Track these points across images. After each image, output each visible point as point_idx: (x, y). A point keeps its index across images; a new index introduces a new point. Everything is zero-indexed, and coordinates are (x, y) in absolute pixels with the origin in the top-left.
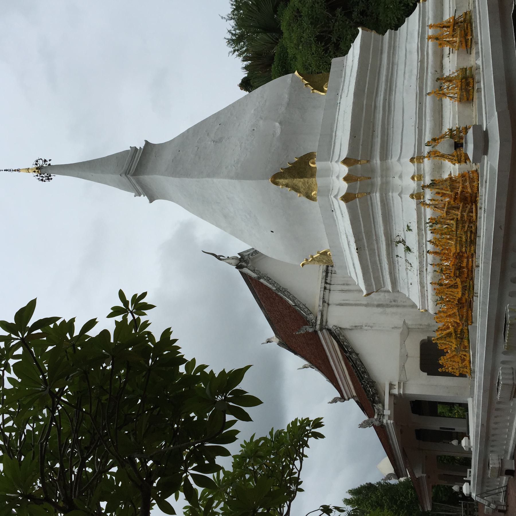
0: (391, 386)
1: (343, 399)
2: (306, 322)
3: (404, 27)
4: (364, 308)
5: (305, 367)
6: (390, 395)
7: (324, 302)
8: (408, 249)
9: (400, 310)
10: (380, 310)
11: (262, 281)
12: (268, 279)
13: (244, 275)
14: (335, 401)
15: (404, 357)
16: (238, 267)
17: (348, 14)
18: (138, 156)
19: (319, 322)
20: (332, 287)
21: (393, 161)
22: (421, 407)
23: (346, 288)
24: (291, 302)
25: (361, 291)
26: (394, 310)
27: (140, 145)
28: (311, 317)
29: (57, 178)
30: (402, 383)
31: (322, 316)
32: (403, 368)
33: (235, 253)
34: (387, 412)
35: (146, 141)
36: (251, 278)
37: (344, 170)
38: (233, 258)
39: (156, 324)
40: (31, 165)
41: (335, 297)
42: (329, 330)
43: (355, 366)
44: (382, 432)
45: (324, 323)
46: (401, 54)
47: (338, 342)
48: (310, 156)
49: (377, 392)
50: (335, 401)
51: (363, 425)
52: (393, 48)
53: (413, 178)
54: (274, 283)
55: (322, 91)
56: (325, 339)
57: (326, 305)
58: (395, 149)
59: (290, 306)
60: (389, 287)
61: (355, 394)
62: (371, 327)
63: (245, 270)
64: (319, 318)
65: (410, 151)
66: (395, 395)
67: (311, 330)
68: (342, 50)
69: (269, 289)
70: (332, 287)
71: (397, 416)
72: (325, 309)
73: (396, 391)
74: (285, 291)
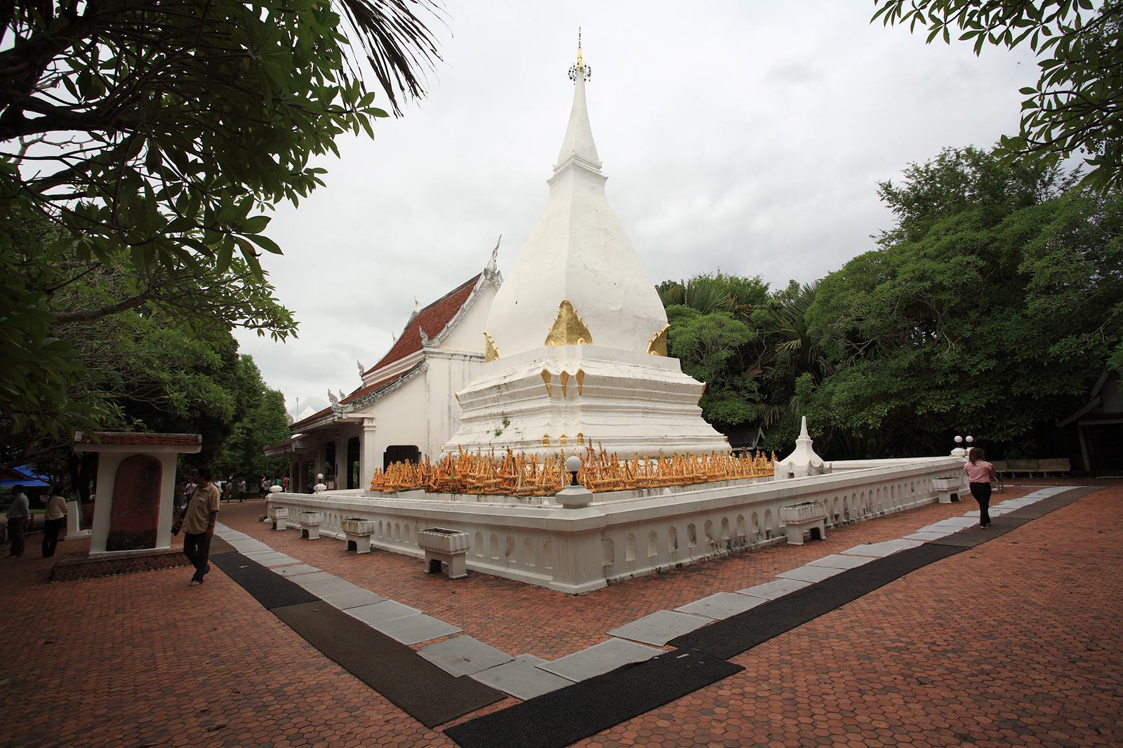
0: (372, 419)
6: (363, 419)
7: (452, 355)
10: (446, 408)
14: (360, 367)
18: (594, 170)
19: (432, 350)
26: (446, 421)
31: (438, 353)
35: (607, 178)
41: (457, 365)
42: (424, 360)
45: (431, 355)
50: (360, 367)
57: (449, 357)
61: (367, 386)
62: (429, 400)
63: (483, 278)
64: (436, 350)
66: (363, 423)
72: (445, 356)
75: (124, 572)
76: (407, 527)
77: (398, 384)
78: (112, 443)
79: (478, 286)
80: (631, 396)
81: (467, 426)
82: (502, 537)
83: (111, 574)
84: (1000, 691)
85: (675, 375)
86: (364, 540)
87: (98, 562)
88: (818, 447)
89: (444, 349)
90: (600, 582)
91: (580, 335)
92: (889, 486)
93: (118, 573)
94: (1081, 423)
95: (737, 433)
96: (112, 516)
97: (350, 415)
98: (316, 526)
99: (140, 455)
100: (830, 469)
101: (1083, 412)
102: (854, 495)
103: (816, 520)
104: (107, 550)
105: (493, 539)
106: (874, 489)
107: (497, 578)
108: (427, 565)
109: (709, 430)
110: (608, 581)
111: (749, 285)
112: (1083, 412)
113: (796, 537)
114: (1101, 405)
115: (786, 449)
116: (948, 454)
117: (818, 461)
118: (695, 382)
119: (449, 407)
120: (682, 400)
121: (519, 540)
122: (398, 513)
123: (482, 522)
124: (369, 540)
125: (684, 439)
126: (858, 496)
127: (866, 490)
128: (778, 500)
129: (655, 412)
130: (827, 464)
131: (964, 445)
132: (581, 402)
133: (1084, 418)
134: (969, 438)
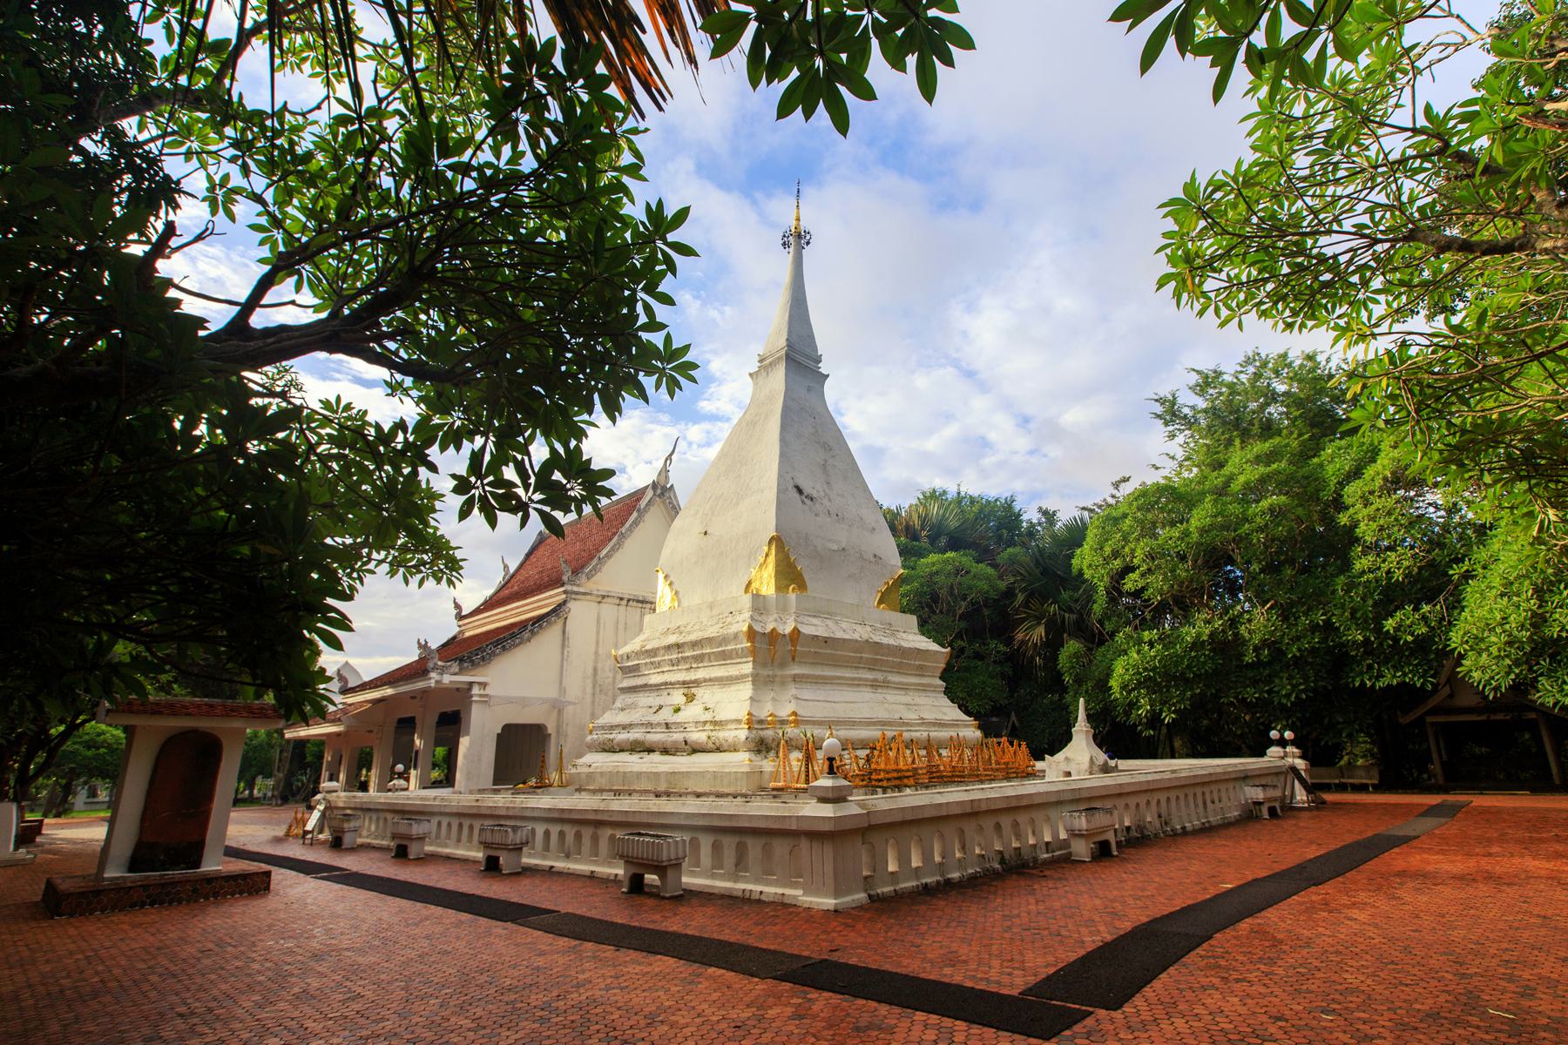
0: (484, 685)
1: (460, 617)
2: (576, 572)
3: (946, 701)
4: (593, 650)
5: (506, 567)
6: (471, 684)
8: (677, 710)
9: (588, 698)
10: (590, 671)
11: (635, 514)
12: (636, 523)
13: (642, 491)
14: (457, 606)
15: (524, 702)
16: (654, 485)
17: (959, 636)
18: (811, 364)
20: (622, 608)
21: (792, 690)
22: (451, 723)
23: (621, 627)
24: (604, 552)
25: (616, 647)
26: (589, 690)
27: (824, 368)
28: (583, 578)
29: (788, 258)
30: (486, 700)
32: (510, 701)
33: (673, 479)
34: (447, 679)
36: (638, 500)
37: (788, 629)
38: (667, 477)
39: (1017, 506)
40: (804, 225)
41: (609, 610)
42: (565, 602)
43: (513, 636)
44: (417, 670)
46: (848, 694)
47: (547, 614)
48: (802, 586)
49: (474, 665)
50: (457, 606)
51: (423, 646)
52: (923, 689)
53: (794, 713)
54: (630, 529)
55: (880, 602)
56: (552, 597)
58: (807, 693)
59: (598, 551)
60: (625, 684)
61: (467, 634)
63: (650, 493)
65: (806, 711)
66: (470, 689)
67: (565, 578)
68: (924, 627)
69: (623, 524)
70: (622, 608)
71: (441, 691)
73: (476, 690)
74: (619, 545)
75: (161, 904)
76: (578, 836)
77: (526, 635)
78: (161, 713)
79: (643, 503)
80: (856, 664)
81: (629, 699)
82: (729, 842)
83: (143, 905)
84: (1314, 987)
85: (911, 637)
86: (513, 855)
87: (119, 888)
88: (1100, 740)
89: (586, 585)
90: (861, 896)
91: (793, 581)
92: (1190, 792)
93: (152, 905)
94: (1429, 719)
95: (990, 719)
96: (143, 819)
97: (446, 678)
98: (421, 839)
99: (195, 731)
100: (1115, 769)
101: (1431, 703)
102: (1148, 803)
103: (1104, 830)
104: (130, 870)
105: (717, 848)
106: (1173, 795)
107: (722, 897)
108: (626, 883)
109: (953, 712)
110: (870, 896)
111: (992, 512)
112: (1431, 703)
113: (1081, 849)
114: (1451, 696)
115: (1058, 741)
116: (1263, 754)
117: (1101, 757)
118: (935, 647)
119: (595, 670)
120: (921, 671)
121: (754, 847)
122: (566, 816)
123: (701, 823)
124: (520, 857)
125: (924, 723)
126: (1154, 804)
127: (1163, 797)
128: (1059, 803)
129: (886, 685)
130: (1112, 763)
131: (1282, 743)
132: (796, 670)
133: (1435, 711)
134: (1288, 735)
